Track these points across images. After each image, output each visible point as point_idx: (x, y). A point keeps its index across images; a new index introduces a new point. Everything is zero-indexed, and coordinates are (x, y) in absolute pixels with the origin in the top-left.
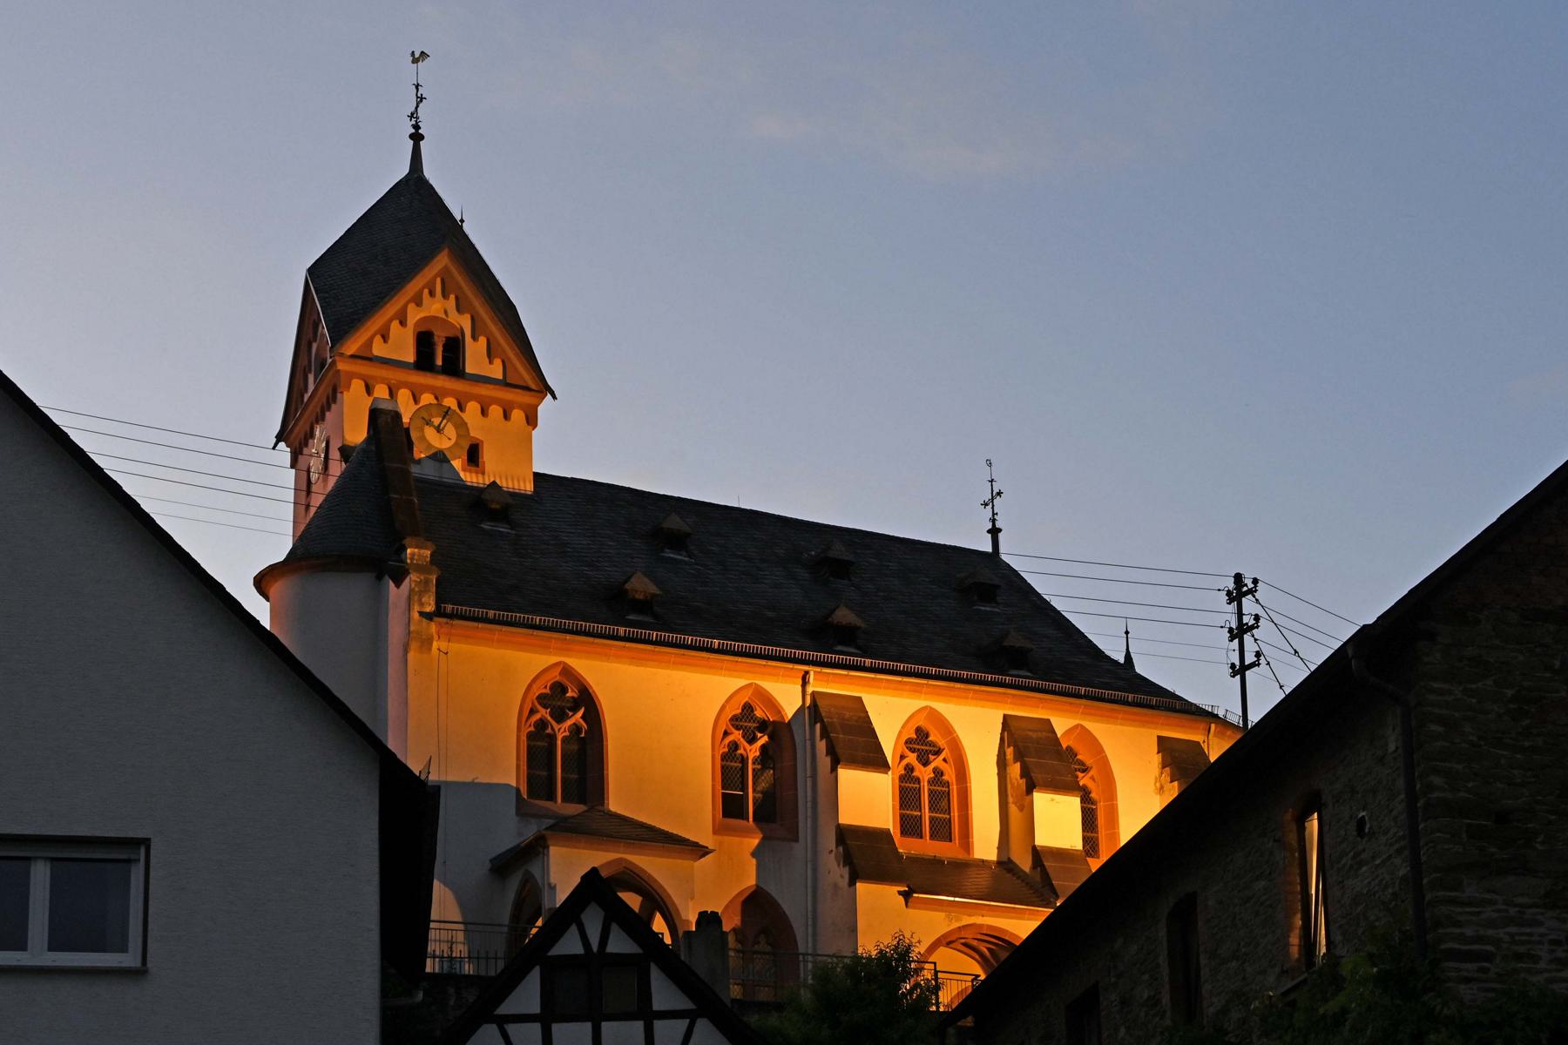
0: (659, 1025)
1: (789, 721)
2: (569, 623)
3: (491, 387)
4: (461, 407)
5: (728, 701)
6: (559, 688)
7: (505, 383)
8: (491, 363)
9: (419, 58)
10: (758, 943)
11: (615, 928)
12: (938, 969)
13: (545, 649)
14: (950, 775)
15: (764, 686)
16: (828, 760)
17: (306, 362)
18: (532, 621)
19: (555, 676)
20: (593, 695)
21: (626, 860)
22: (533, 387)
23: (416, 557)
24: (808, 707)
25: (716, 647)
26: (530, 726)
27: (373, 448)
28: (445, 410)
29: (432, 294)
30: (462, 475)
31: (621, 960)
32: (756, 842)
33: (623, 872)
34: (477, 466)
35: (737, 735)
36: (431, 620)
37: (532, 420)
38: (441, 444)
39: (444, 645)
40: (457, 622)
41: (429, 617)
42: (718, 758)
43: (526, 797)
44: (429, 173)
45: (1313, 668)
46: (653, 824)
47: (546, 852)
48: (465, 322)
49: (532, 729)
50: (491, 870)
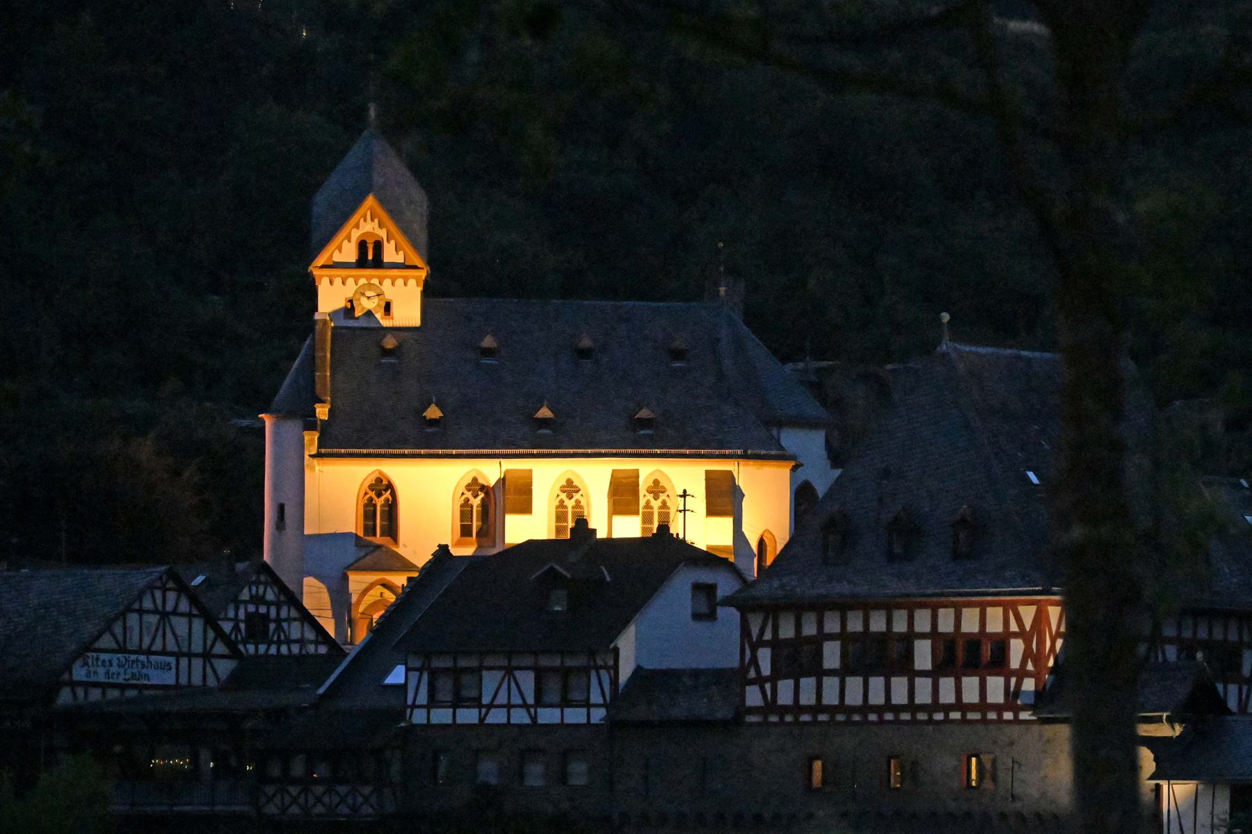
6: (379, 480)
8: (397, 254)
14: (583, 503)
21: (385, 579)
29: (365, 220)
30: (381, 321)
45: (329, 608)
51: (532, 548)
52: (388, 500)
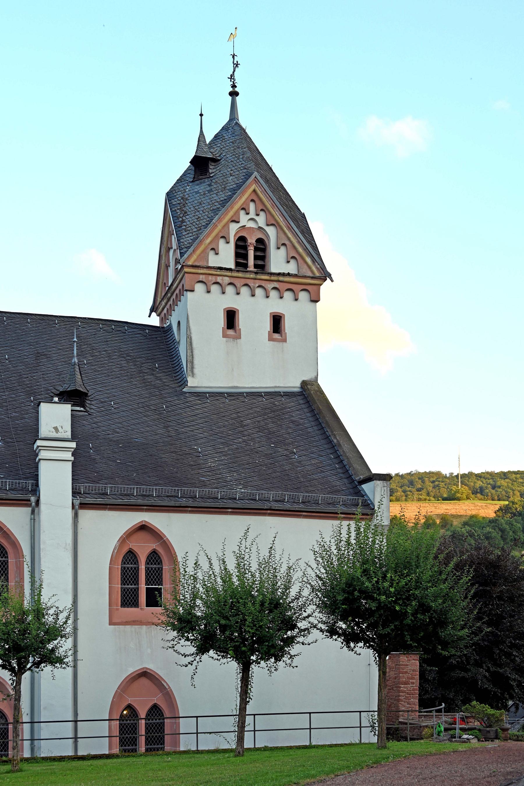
12: (362, 713)
37: (315, 300)
44: (243, 122)
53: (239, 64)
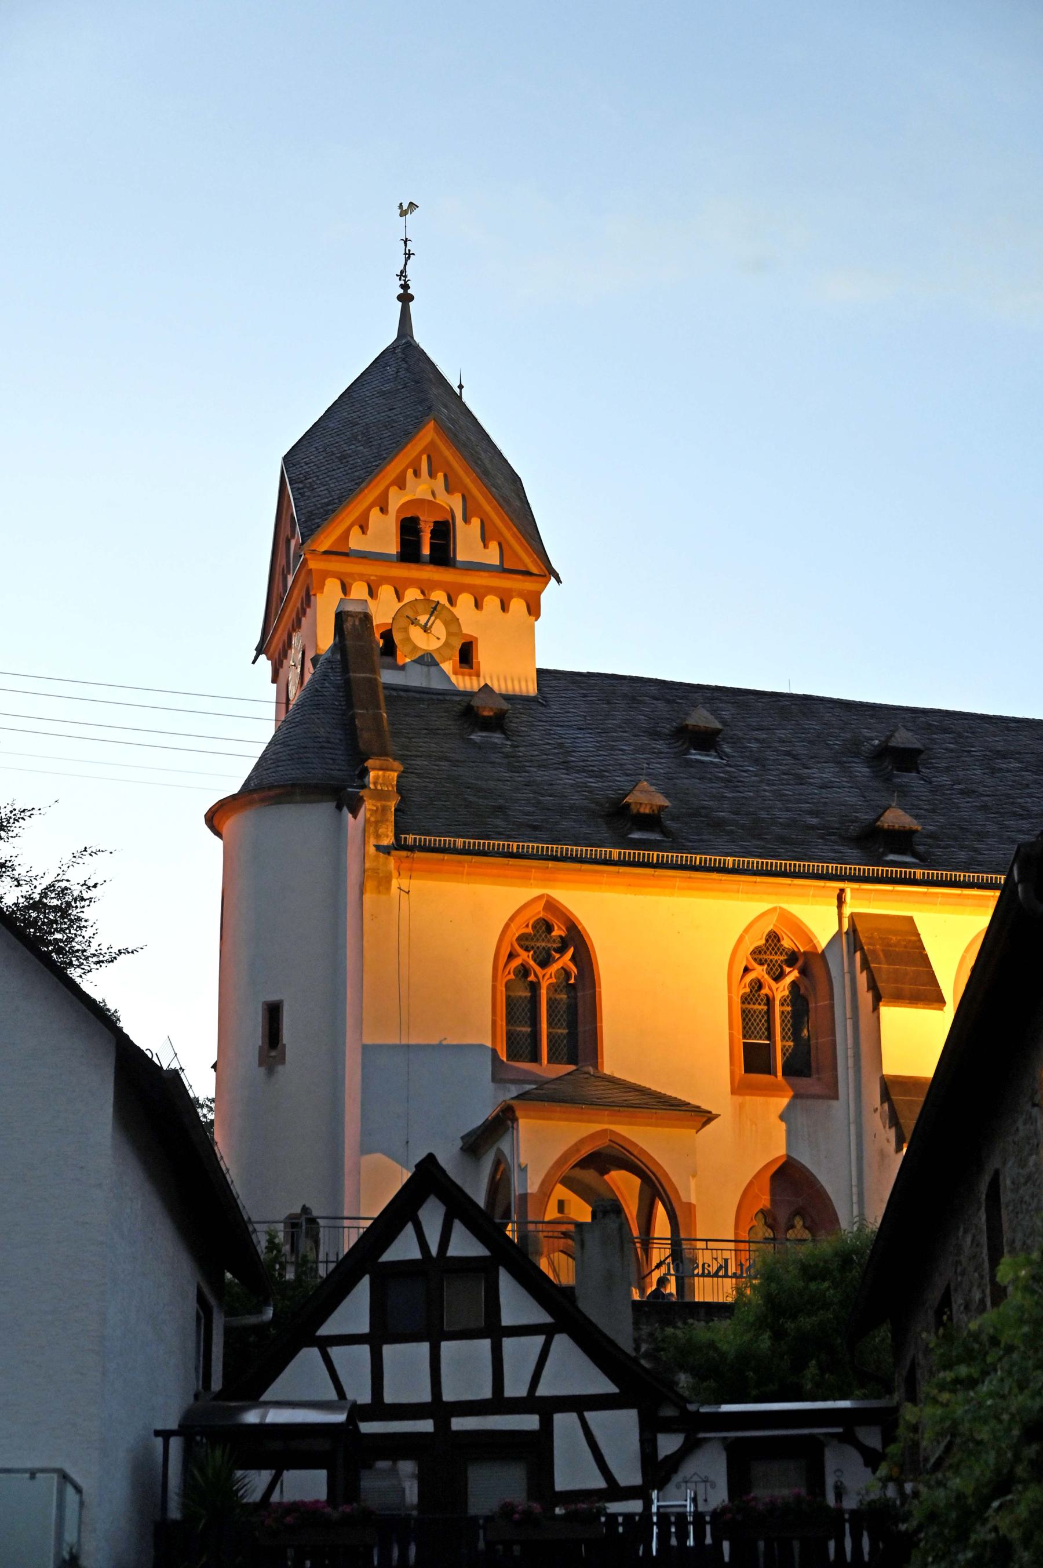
0: (508, 1343)
1: (823, 951)
2: (556, 848)
3: (486, 574)
4: (451, 601)
5: (747, 930)
7: (503, 570)
8: (486, 546)
9: (407, 210)
10: (793, 1227)
11: (458, 1227)
13: (525, 879)
15: (789, 909)
16: (869, 996)
17: (284, 562)
18: (508, 848)
19: (538, 911)
20: (582, 933)
21: (612, 1132)
22: (534, 570)
23: (380, 781)
24: (847, 933)
25: (731, 866)
26: (509, 973)
27: (339, 657)
28: (433, 606)
29: (417, 474)
30: (453, 679)
31: (465, 1265)
32: (785, 1101)
33: (609, 1146)
34: (471, 667)
35: (760, 972)
36: (389, 853)
37: (534, 609)
38: (428, 645)
39: (405, 883)
40: (418, 855)
41: (386, 850)
42: (737, 1000)
43: (505, 1059)
44: (420, 336)
46: (648, 1086)
47: (515, 1126)
48: (456, 503)
49: (512, 976)
50: (461, 1148)
51: (421, 1495)
52: (568, 974)
53: (397, 275)
